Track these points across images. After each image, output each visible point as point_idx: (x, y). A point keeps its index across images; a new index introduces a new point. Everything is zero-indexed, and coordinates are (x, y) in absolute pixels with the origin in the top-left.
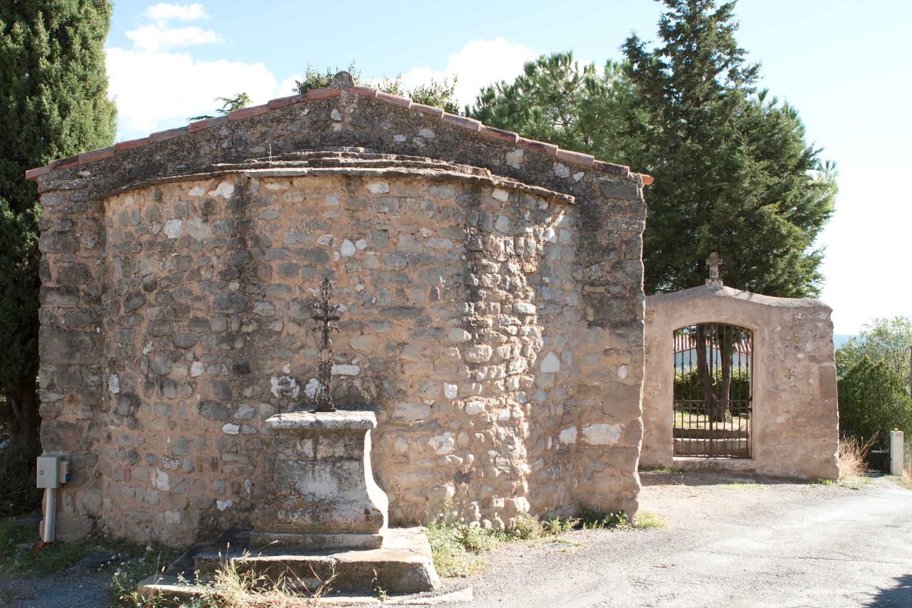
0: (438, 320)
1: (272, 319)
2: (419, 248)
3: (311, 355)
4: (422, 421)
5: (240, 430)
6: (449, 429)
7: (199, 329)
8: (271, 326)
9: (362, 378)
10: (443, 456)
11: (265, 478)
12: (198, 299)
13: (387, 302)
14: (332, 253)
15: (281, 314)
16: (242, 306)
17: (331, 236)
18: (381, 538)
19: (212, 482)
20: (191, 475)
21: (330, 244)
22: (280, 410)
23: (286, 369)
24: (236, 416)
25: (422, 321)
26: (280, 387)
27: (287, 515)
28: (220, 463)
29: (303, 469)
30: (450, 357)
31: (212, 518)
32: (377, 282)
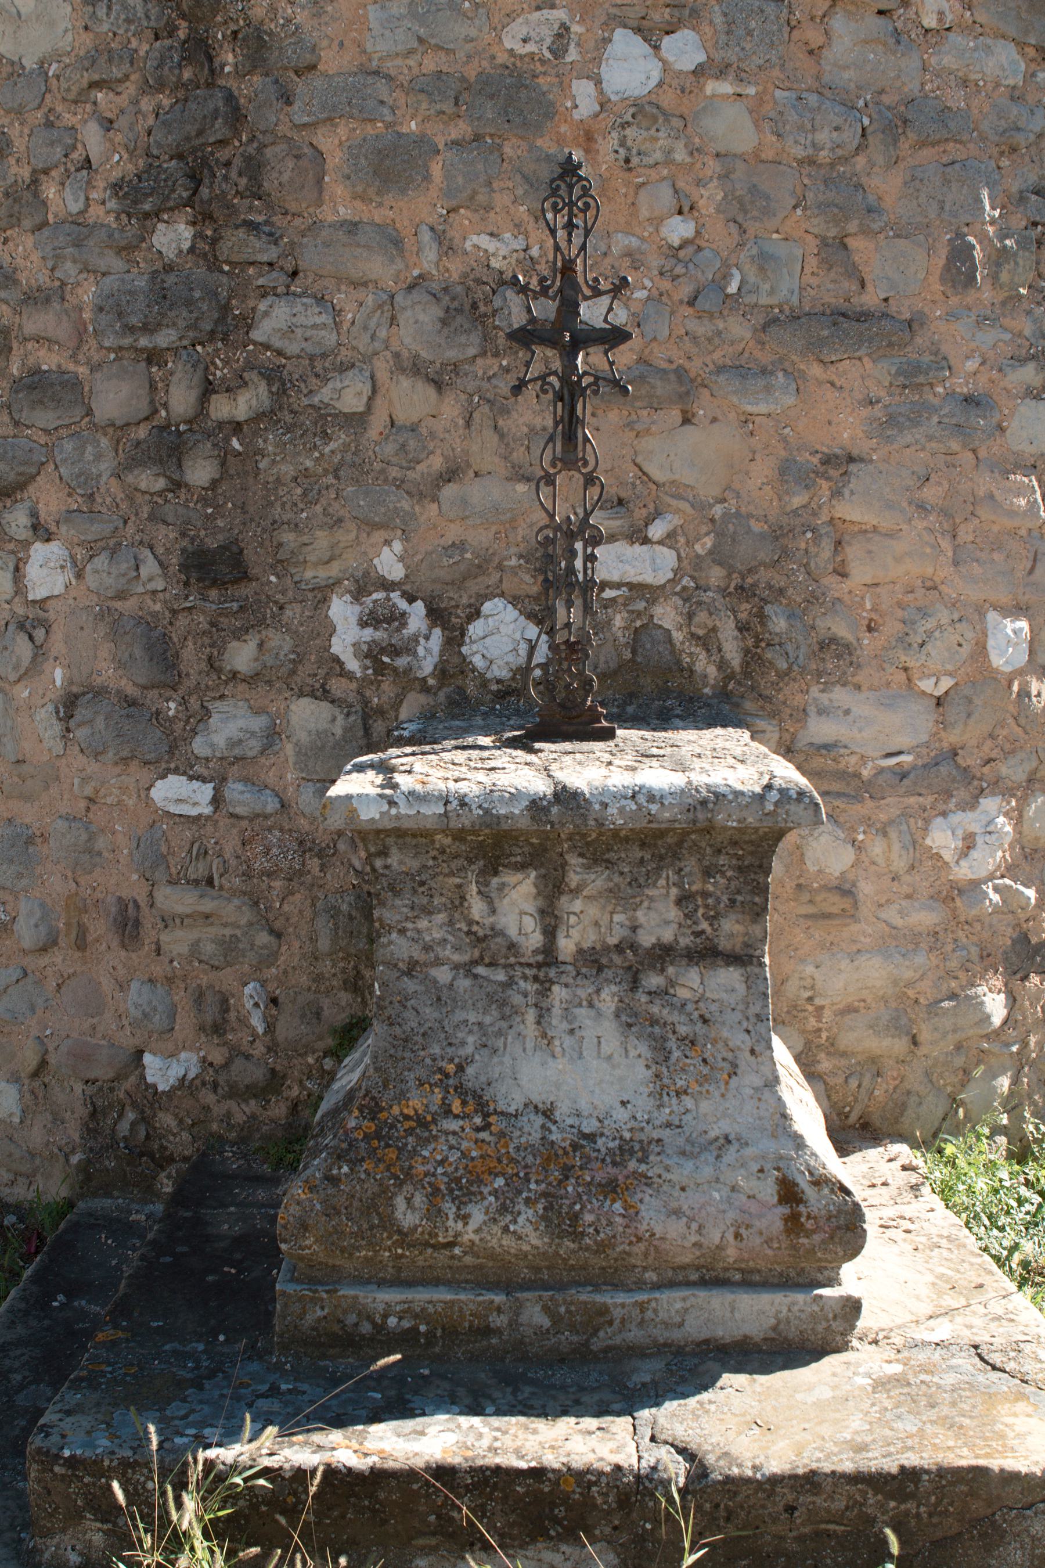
0: (971, 365)
1: (328, 364)
2: (904, 73)
3: (496, 506)
4: (907, 759)
5: (217, 801)
6: (997, 786)
7: (45, 418)
8: (325, 394)
9: (685, 595)
10: (975, 884)
11: (318, 978)
12: (36, 299)
13: (783, 293)
14: (564, 87)
15: (363, 343)
16: (205, 316)
17: (560, 14)
18: (853, 1307)
19: (122, 986)
20: (44, 960)
21: (558, 51)
22: (371, 733)
23: (389, 563)
24: (199, 746)
25: (917, 369)
26: (368, 634)
27: (434, 1212)
28: (149, 920)
29: (498, 1000)
30: (1013, 513)
31: (131, 1115)
32: (744, 208)
